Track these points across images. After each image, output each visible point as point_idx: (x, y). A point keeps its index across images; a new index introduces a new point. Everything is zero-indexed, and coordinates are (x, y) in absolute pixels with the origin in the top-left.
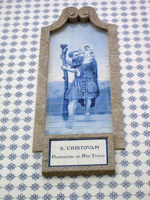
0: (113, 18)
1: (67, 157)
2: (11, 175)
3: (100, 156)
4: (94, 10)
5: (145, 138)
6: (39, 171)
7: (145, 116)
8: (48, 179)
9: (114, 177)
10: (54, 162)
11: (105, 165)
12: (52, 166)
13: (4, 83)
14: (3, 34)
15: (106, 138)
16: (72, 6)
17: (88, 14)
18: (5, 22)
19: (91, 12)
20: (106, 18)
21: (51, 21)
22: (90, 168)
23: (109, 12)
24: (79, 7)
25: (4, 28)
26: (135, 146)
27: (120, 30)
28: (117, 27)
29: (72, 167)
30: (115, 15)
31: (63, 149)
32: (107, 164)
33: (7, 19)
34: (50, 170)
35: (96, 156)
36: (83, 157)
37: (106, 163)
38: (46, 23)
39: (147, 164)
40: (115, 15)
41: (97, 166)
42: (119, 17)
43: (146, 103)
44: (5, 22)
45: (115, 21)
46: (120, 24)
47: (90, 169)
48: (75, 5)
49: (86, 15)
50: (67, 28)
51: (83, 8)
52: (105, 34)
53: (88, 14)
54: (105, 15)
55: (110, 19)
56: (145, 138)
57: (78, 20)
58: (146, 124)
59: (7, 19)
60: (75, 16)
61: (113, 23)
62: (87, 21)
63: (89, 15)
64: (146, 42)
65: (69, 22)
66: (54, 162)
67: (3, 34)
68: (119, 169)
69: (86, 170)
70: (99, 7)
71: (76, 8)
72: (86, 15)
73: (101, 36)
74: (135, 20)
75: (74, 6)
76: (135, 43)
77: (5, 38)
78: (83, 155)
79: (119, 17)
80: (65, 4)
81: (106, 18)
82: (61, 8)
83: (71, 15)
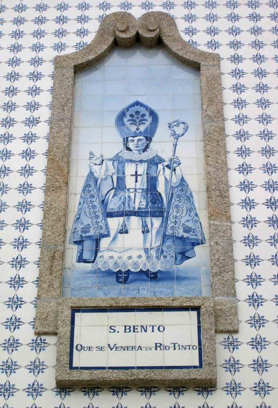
0: (209, 38)
1: (131, 349)
2: (16, 286)
3: (188, 348)
4: (171, 20)
5: (269, 213)
6: (48, 379)
7: (268, 152)
8: (63, 396)
9: (181, 396)
10: (81, 359)
11: (195, 367)
12: (77, 368)
13: (7, 41)
14: (8, 84)
15: (197, 309)
16: (118, 10)
17: (158, 30)
18: (11, 55)
19: (164, 24)
20: (195, 38)
21: (71, 43)
22: (106, 375)
23: (201, 24)
24: (137, 12)
25: (9, 69)
26: (255, 327)
27: (227, 67)
28: (217, 59)
29: (164, 372)
30: (212, 31)
31: (115, 331)
32: (71, 367)
33: (16, 48)
34: (76, 376)
35: (181, 348)
36: (156, 349)
37: (197, 364)
38: (59, 47)
39: (254, 368)
40: (212, 31)
41: (157, 371)
42: (224, 38)
43: (272, 144)
44: (11, 55)
45: (214, 45)
46: (225, 52)
47: (97, 375)
48: (126, 9)
49: (154, 30)
50: (112, 58)
51: (146, 17)
52: (195, 75)
53: (158, 30)
54: (191, 32)
55: (201, 41)
56: (269, 213)
57: (138, 42)
58: (269, 169)
59: (16, 48)
60: (131, 34)
61: (210, 51)
62: (158, 43)
63: (160, 30)
64: (268, 195)
65: (117, 45)
66: (81, 359)
67: (8, 84)
68: (224, 378)
69: (124, 378)
70: (178, 13)
71: (130, 15)
72: (154, 30)
73: (183, 75)
74: (234, 31)
75: (123, 10)
76: (259, 96)
77: (11, 91)
78: (156, 344)
79: (224, 38)
80: (104, 6)
81: (195, 38)
82: (94, 13)
83: (120, 31)
